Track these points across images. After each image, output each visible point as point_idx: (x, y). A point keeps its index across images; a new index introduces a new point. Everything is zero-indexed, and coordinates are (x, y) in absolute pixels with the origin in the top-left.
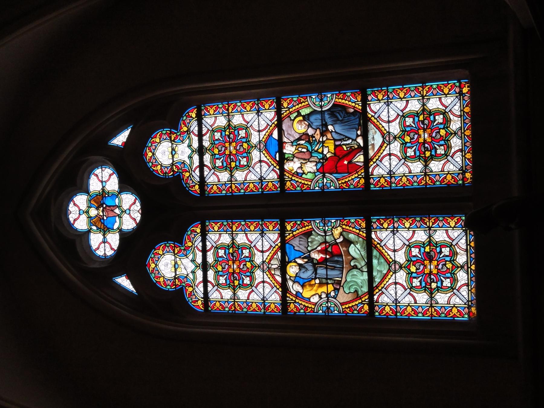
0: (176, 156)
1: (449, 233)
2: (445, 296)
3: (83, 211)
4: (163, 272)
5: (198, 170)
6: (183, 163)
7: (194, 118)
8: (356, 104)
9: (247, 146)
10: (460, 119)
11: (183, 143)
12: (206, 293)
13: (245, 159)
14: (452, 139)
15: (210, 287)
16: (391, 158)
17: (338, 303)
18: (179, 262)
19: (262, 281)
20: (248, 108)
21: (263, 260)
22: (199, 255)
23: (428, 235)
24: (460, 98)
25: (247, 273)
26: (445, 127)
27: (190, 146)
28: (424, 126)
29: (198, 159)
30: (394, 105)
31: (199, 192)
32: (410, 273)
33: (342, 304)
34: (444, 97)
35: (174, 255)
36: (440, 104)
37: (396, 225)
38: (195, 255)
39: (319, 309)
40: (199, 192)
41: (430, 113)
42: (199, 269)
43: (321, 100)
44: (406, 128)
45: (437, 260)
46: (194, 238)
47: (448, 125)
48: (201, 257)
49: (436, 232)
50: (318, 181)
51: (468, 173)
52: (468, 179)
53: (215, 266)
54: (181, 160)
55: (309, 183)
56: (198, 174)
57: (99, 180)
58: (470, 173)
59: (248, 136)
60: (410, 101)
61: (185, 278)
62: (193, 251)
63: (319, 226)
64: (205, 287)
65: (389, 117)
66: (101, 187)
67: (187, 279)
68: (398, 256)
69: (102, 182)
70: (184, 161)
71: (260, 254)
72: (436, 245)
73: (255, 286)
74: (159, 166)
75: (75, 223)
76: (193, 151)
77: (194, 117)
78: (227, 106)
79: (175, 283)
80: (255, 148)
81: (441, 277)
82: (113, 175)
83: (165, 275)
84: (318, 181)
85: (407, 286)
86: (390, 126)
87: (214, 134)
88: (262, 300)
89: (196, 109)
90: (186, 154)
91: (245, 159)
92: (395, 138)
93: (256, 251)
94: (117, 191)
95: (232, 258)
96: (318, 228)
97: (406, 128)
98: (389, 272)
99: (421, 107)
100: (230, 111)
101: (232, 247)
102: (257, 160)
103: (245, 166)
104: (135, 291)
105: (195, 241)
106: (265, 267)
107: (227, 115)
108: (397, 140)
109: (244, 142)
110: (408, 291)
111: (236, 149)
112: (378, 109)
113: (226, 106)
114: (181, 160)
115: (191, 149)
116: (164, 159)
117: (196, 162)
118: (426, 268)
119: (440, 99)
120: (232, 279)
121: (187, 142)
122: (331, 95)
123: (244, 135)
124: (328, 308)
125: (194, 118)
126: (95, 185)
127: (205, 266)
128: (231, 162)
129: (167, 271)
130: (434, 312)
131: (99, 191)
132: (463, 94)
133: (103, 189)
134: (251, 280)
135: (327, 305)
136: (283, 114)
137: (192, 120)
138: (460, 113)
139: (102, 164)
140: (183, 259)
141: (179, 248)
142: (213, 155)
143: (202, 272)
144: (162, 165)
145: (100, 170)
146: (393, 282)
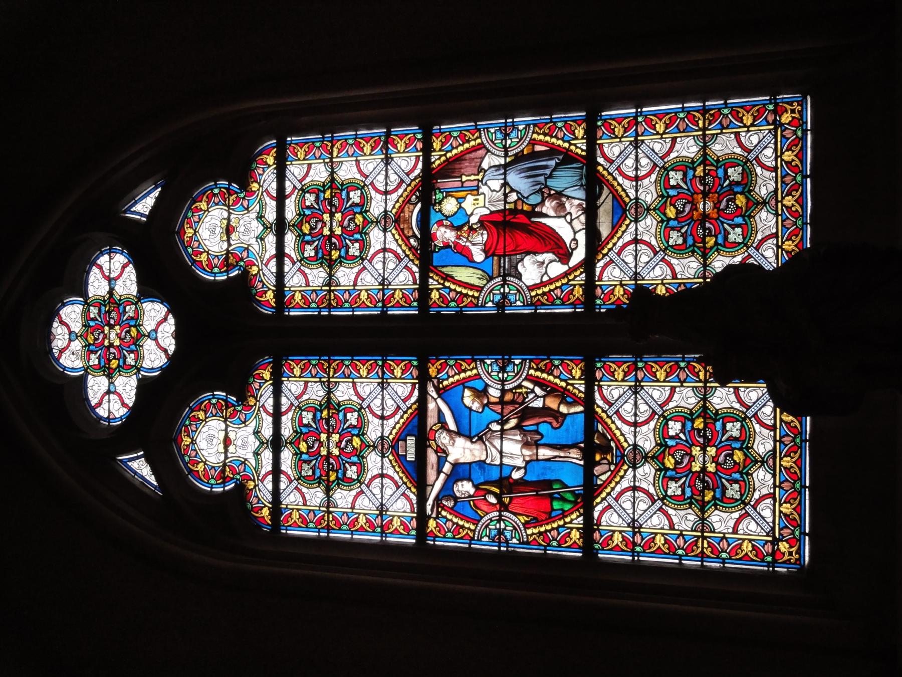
0: (231, 449)
2: (729, 517)
3: (76, 334)
4: (207, 242)
5: (274, 261)
6: (244, 462)
7: (270, 166)
8: (568, 384)
9: (359, 443)
10: (772, 433)
11: (246, 426)
12: (276, 492)
13: (357, 245)
14: (756, 472)
15: (288, 264)
16: (634, 173)
17: (523, 285)
18: (232, 435)
19: (379, 474)
20: (364, 372)
21: (382, 433)
22: (271, 205)
23: (702, 144)
24: (776, 132)
25: (352, 458)
27: (256, 433)
28: (705, 188)
29: (271, 457)
31: (270, 523)
32: (664, 221)
33: (531, 288)
35: (225, 421)
37: (640, 375)
38: (262, 207)
39: (484, 534)
40: (270, 523)
42: (266, 448)
43: (503, 369)
46: (259, 390)
48: (271, 426)
49: (716, 390)
50: (492, 290)
51: (783, 541)
52: (784, 554)
53: (295, 443)
54: (239, 457)
55: (476, 294)
56: (274, 270)
57: (105, 276)
58: (788, 543)
59: (365, 201)
61: (241, 464)
62: (257, 414)
63: (490, 371)
64: (276, 482)
66: (107, 289)
67: (248, 253)
68: (642, 436)
69: (109, 279)
70: (246, 460)
71: (377, 421)
72: (716, 417)
73: (368, 258)
74: (204, 255)
75: (61, 355)
76: (262, 443)
77: (271, 164)
78: (330, 144)
79: (224, 474)
80: (377, 224)
81: (725, 225)
82: (128, 265)
83: (208, 459)
84: (492, 290)
87: (304, 196)
88: (380, 284)
89: (275, 150)
90: (253, 232)
91: (357, 245)
93: (370, 416)
94: (136, 297)
95: (326, 428)
96: (493, 142)
98: (623, 218)
100: (335, 154)
101: (331, 187)
102: (379, 247)
103: (357, 257)
104: (152, 479)
105: (261, 396)
106: (388, 221)
107: (327, 381)
109: (354, 435)
110: (660, 163)
111: (339, 447)
113: (327, 145)
114: (242, 243)
115: (259, 439)
116: (210, 451)
117: (267, 465)
118: (694, 461)
119: (737, 135)
120: (328, 248)
121: (253, 424)
122: (524, 126)
123: (357, 200)
124: (504, 296)
125: (266, 381)
126: (97, 286)
127: (276, 443)
128: (331, 250)
129: (210, 451)
130: (707, 549)
131: (104, 297)
132: (782, 125)
133: (111, 292)
134: (361, 249)
135: (498, 526)
136: (434, 162)
137: (264, 383)
138: (774, 163)
139: (109, 245)
140: (240, 428)
141: (232, 408)
142: (298, 454)
143: (271, 454)
144: (210, 252)
145: (106, 257)
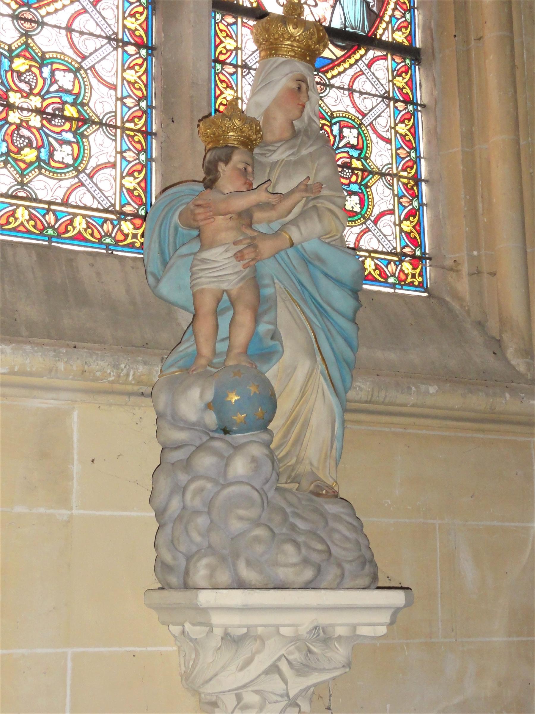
1: (390, 216)
26: (42, 163)
30: (383, 111)
34: (395, 221)
36: (382, 210)
41: (80, 136)
44: (338, 124)
45: (41, 128)
47: (46, 170)
60: (389, 146)
65: (82, 33)
85: (368, 130)
86: (58, 30)
92: (26, 35)
97: (338, 124)
99: (379, 169)
108: (20, 37)
112: (103, 13)
146: (67, 35)
